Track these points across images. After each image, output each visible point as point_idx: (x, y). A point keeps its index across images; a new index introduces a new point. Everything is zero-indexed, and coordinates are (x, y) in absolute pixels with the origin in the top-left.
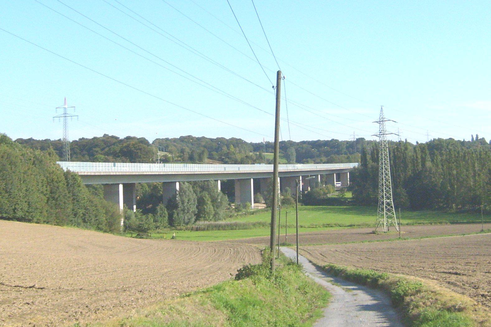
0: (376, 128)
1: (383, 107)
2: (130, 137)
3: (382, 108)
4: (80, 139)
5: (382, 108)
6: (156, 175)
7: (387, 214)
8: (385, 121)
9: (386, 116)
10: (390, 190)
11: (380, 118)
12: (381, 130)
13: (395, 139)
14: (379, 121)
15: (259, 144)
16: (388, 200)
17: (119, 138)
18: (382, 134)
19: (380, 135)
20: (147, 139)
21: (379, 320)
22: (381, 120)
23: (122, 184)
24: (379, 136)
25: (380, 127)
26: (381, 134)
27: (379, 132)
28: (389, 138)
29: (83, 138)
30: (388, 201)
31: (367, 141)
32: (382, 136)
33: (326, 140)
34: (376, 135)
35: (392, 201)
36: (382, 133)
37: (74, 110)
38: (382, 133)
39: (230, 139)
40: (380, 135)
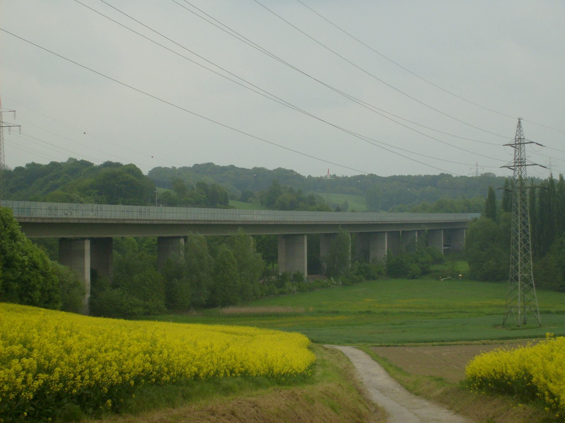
0: (509, 156)
1: (521, 121)
2: (119, 163)
3: (519, 122)
4: (28, 165)
5: (519, 122)
6: (147, 224)
7: (522, 286)
8: (524, 143)
9: (528, 135)
10: (529, 238)
11: (515, 138)
12: (517, 158)
13: (543, 175)
14: (514, 143)
15: (302, 176)
16: (526, 273)
17: (93, 164)
18: (517, 166)
19: (514, 166)
20: (138, 166)
21: (523, 200)
22: (517, 143)
23: (89, 239)
24: (513, 168)
25: (515, 153)
26: (517, 164)
27: (513, 161)
28: (531, 172)
29: (33, 164)
30: (526, 275)
31: (499, 177)
32: (518, 169)
33: (423, 174)
34: (509, 167)
35: (532, 275)
36: (520, 163)
37: (15, 116)
38: (520, 163)
39: (274, 170)
40: (514, 166)
